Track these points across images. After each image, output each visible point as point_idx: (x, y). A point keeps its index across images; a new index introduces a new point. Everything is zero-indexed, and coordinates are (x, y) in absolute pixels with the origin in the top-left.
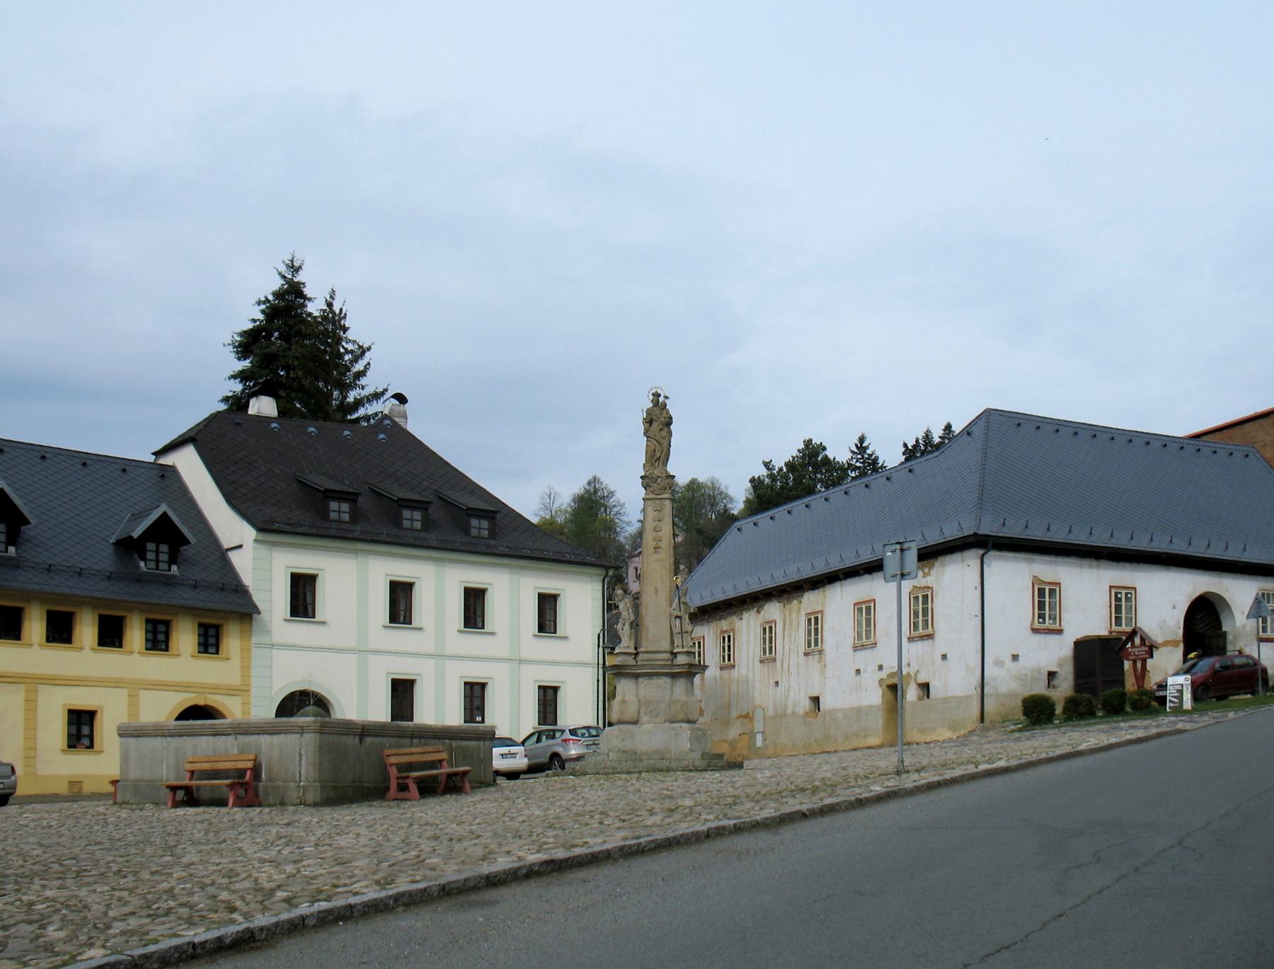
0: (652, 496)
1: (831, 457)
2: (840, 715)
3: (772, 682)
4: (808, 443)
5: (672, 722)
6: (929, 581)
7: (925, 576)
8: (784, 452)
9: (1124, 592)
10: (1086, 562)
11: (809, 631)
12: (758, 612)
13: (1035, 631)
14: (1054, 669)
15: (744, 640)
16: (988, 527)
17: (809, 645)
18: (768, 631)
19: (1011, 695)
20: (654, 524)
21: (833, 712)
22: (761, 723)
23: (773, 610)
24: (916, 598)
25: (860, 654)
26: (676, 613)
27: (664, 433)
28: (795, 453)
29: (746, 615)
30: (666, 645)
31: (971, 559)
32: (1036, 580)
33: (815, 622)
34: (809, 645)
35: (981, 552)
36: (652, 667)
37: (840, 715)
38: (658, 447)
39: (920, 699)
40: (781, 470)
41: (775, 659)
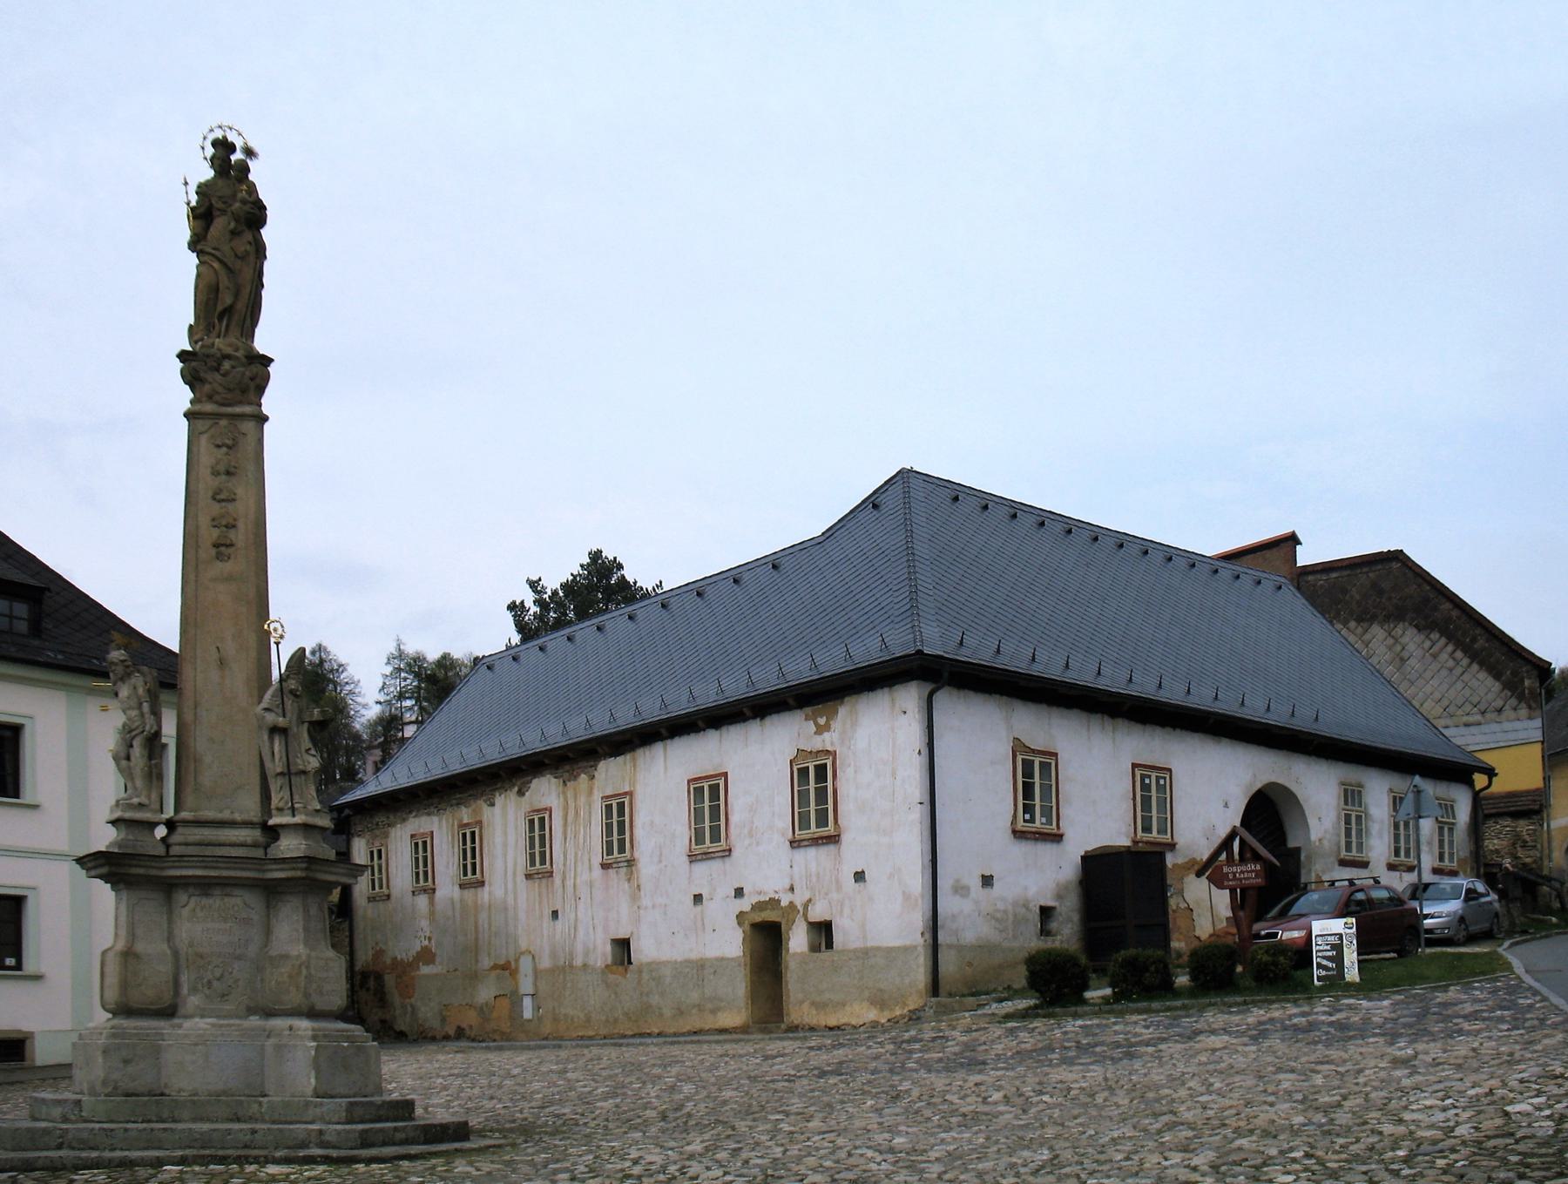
0: (209, 407)
1: (630, 579)
2: (667, 972)
3: (547, 912)
4: (596, 556)
5: (269, 1014)
6: (828, 741)
7: (820, 730)
8: (559, 571)
9: (1154, 775)
10: (1096, 720)
11: (609, 827)
12: (521, 793)
13: (1018, 834)
14: (1050, 903)
15: (498, 840)
16: (936, 642)
17: (610, 852)
18: (538, 825)
19: (984, 948)
20: (214, 483)
21: (654, 966)
22: (530, 979)
23: (545, 790)
24: (804, 772)
25: (702, 868)
26: (271, 718)
27: (242, 245)
28: (576, 570)
29: (499, 800)
30: (248, 805)
31: (909, 697)
32: (1018, 747)
33: (618, 815)
34: (610, 852)
35: (929, 687)
36: (204, 861)
37: (667, 972)
38: (224, 281)
39: (815, 948)
40: (555, 593)
41: (551, 874)
